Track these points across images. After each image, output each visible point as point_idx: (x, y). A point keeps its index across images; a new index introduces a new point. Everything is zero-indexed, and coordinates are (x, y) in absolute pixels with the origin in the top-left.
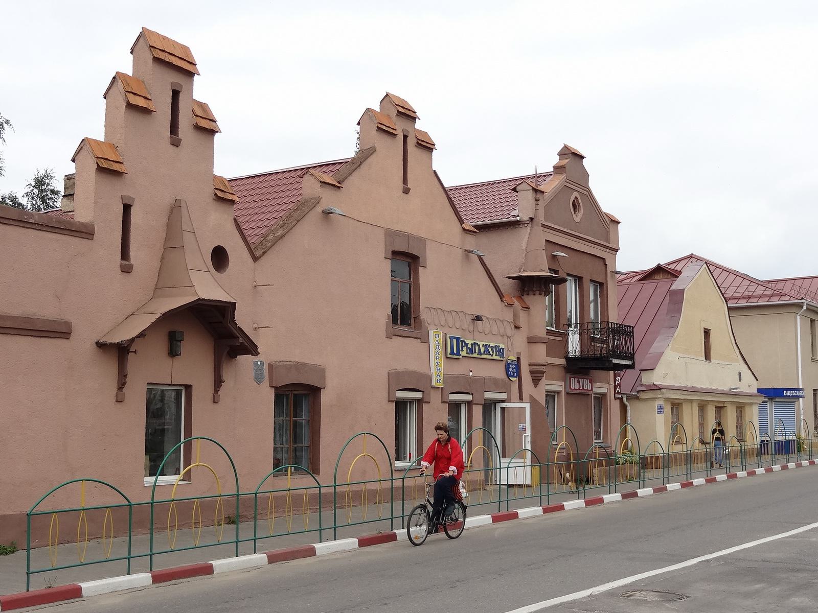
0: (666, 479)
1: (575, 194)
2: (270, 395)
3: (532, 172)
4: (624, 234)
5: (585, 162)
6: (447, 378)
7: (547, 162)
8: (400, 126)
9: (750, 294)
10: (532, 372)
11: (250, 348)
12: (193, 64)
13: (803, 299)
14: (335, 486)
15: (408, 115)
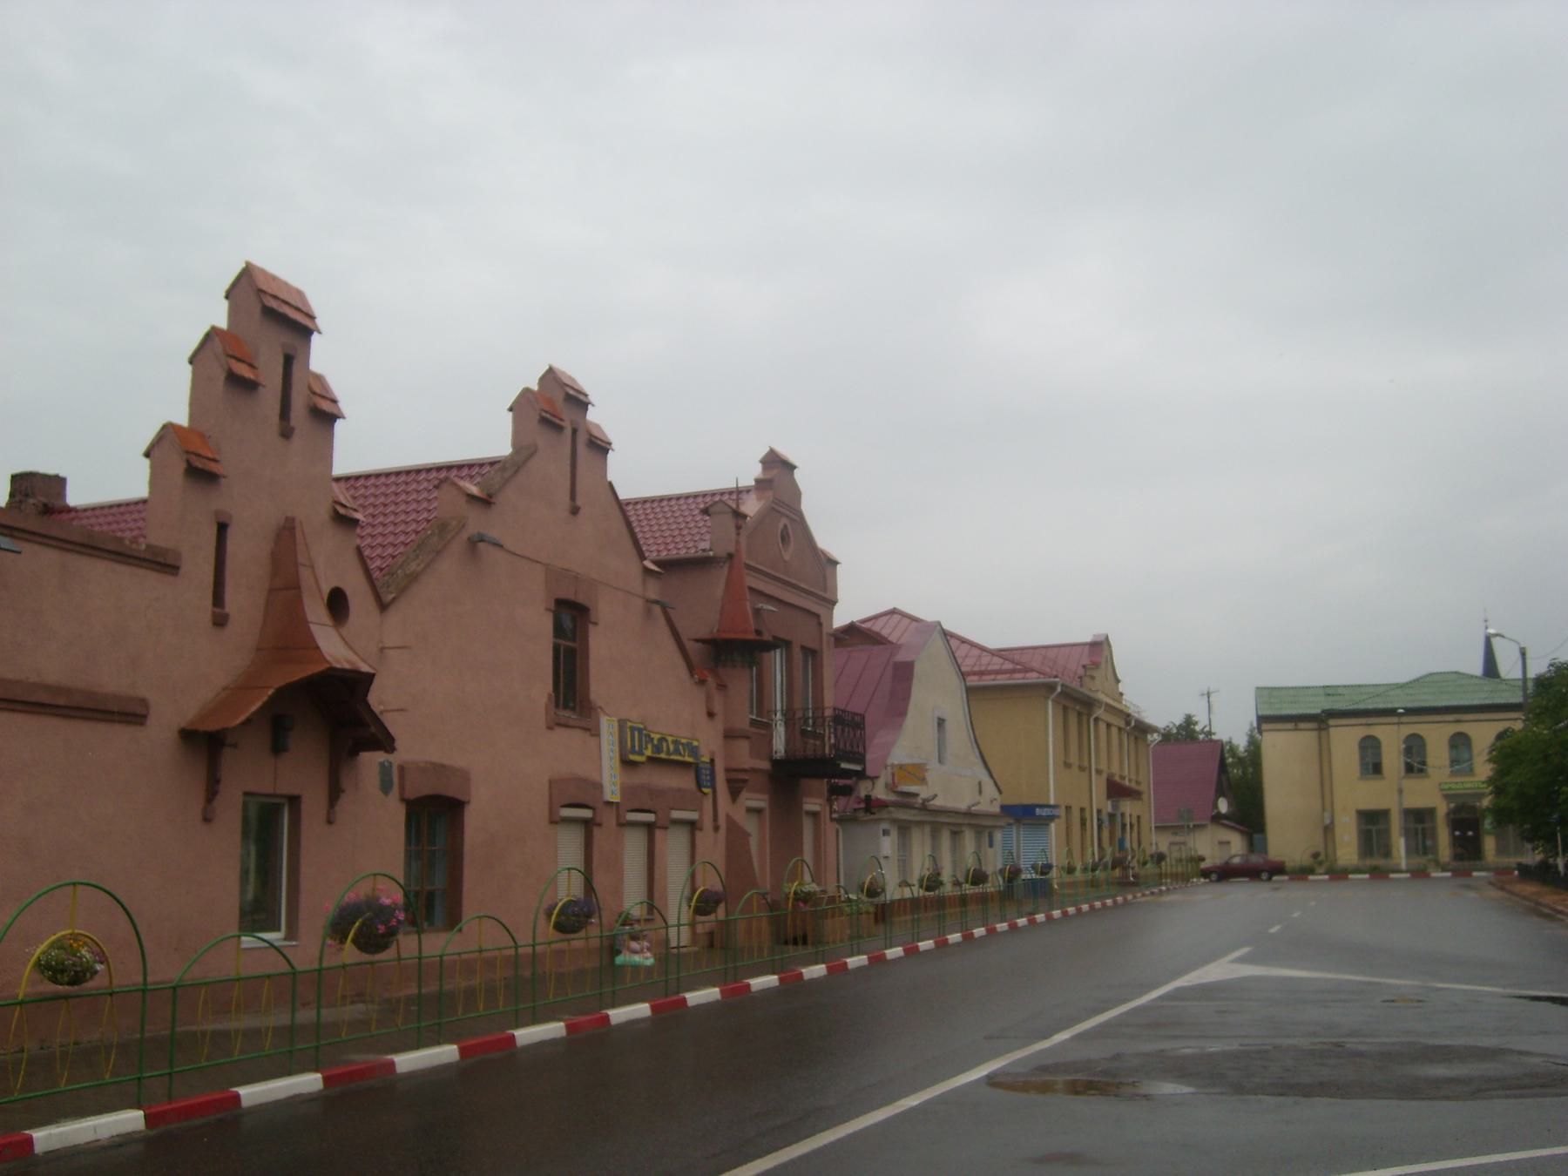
0: (888, 942)
1: (784, 521)
2: (399, 813)
3: (732, 485)
4: (1235, 742)
5: (797, 474)
6: (626, 791)
7: (749, 473)
8: (567, 416)
9: (983, 668)
10: (729, 781)
11: (384, 741)
12: (312, 317)
13: (1056, 677)
14: (533, 946)
15: (579, 402)
